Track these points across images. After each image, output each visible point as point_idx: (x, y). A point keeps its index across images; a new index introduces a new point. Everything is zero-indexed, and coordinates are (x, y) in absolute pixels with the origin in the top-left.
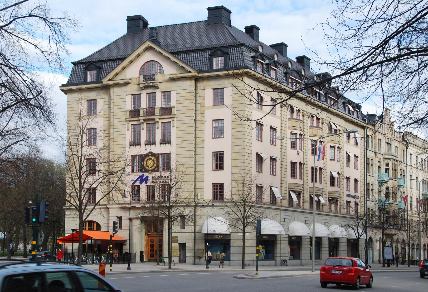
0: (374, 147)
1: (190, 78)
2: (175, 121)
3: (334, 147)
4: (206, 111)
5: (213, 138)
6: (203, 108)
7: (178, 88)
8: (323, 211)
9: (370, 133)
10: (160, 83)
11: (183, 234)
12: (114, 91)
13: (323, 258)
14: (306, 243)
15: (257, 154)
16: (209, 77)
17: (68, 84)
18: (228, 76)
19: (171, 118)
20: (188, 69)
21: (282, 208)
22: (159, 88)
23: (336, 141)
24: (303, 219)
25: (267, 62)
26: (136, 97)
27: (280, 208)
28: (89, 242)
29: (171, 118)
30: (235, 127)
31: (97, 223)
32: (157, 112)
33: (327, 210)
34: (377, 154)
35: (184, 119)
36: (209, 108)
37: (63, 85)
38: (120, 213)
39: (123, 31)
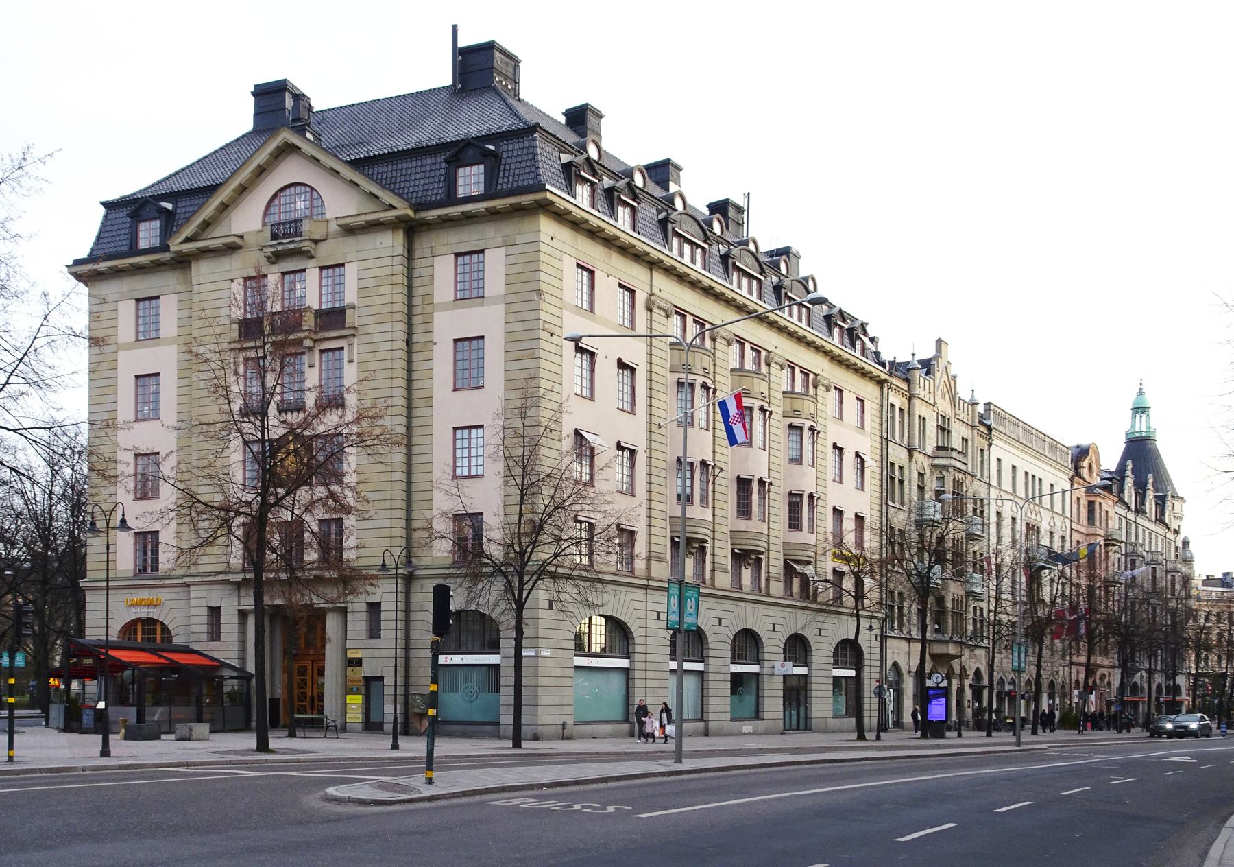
0: (906, 435)
1: (392, 225)
2: (356, 346)
3: (801, 428)
4: (439, 317)
5: (455, 390)
6: (428, 308)
7: (363, 255)
8: (768, 595)
9: (897, 400)
10: (316, 242)
11: (377, 653)
12: (203, 270)
13: (766, 715)
14: (421, 672)
15: (577, 433)
16: (445, 221)
17: (92, 258)
18: (494, 215)
19: (345, 337)
20: (387, 197)
21: (651, 583)
22: (312, 257)
23: (806, 411)
24: (714, 613)
25: (607, 182)
26: (255, 281)
27: (645, 583)
28: (128, 673)
29: (345, 337)
30: (512, 356)
31: (162, 624)
32: (309, 322)
33: (781, 594)
34: (916, 454)
35: (377, 338)
36: (445, 307)
37: (78, 262)
38: (216, 597)
39: (246, 124)
